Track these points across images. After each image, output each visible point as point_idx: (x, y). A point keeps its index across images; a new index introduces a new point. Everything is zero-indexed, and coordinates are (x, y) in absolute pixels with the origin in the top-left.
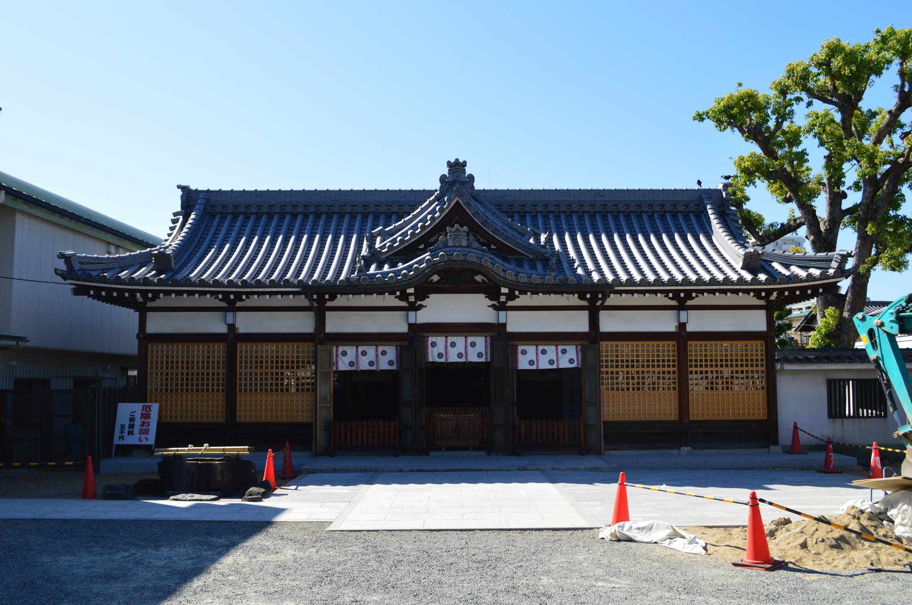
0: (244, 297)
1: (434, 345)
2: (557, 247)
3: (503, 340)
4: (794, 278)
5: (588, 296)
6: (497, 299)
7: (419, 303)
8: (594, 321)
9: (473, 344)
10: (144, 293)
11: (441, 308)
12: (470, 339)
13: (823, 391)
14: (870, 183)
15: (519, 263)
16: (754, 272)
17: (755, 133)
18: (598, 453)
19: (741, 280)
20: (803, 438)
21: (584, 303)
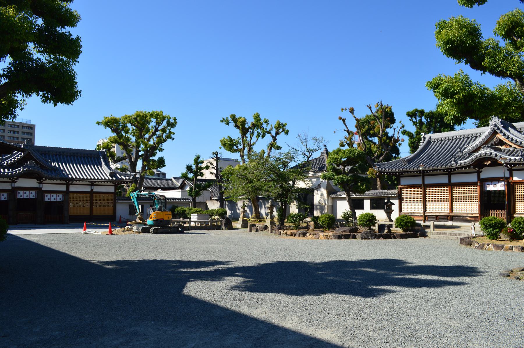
2: (57, 166)
3: (40, 192)
4: (122, 179)
6: (40, 181)
8: (68, 188)
9: (32, 193)
12: (31, 192)
13: (128, 207)
14: (146, 151)
15: (48, 172)
16: (112, 177)
17: (115, 130)
18: (68, 224)
19: (109, 179)
20: (122, 219)
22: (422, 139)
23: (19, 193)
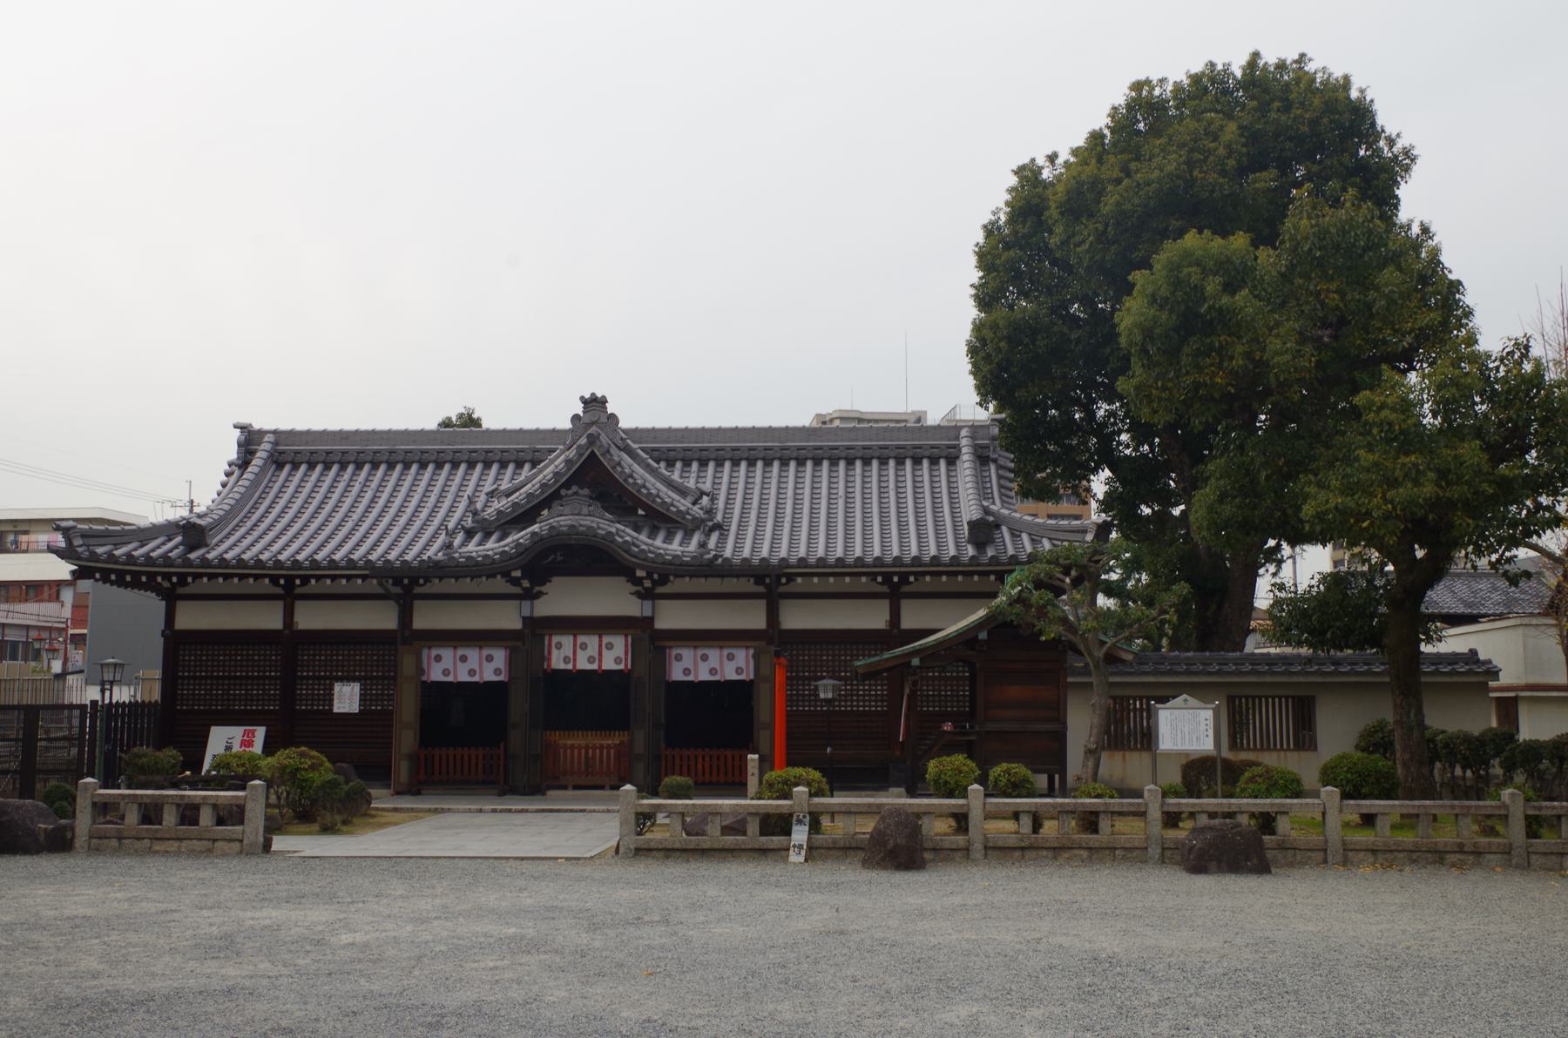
0: (190, 580)
1: (559, 646)
3: (652, 642)
5: (282, 582)
7: (537, 589)
10: (167, 576)
11: (566, 598)
21: (761, 589)
22: (1402, 493)
23: (679, 658)
